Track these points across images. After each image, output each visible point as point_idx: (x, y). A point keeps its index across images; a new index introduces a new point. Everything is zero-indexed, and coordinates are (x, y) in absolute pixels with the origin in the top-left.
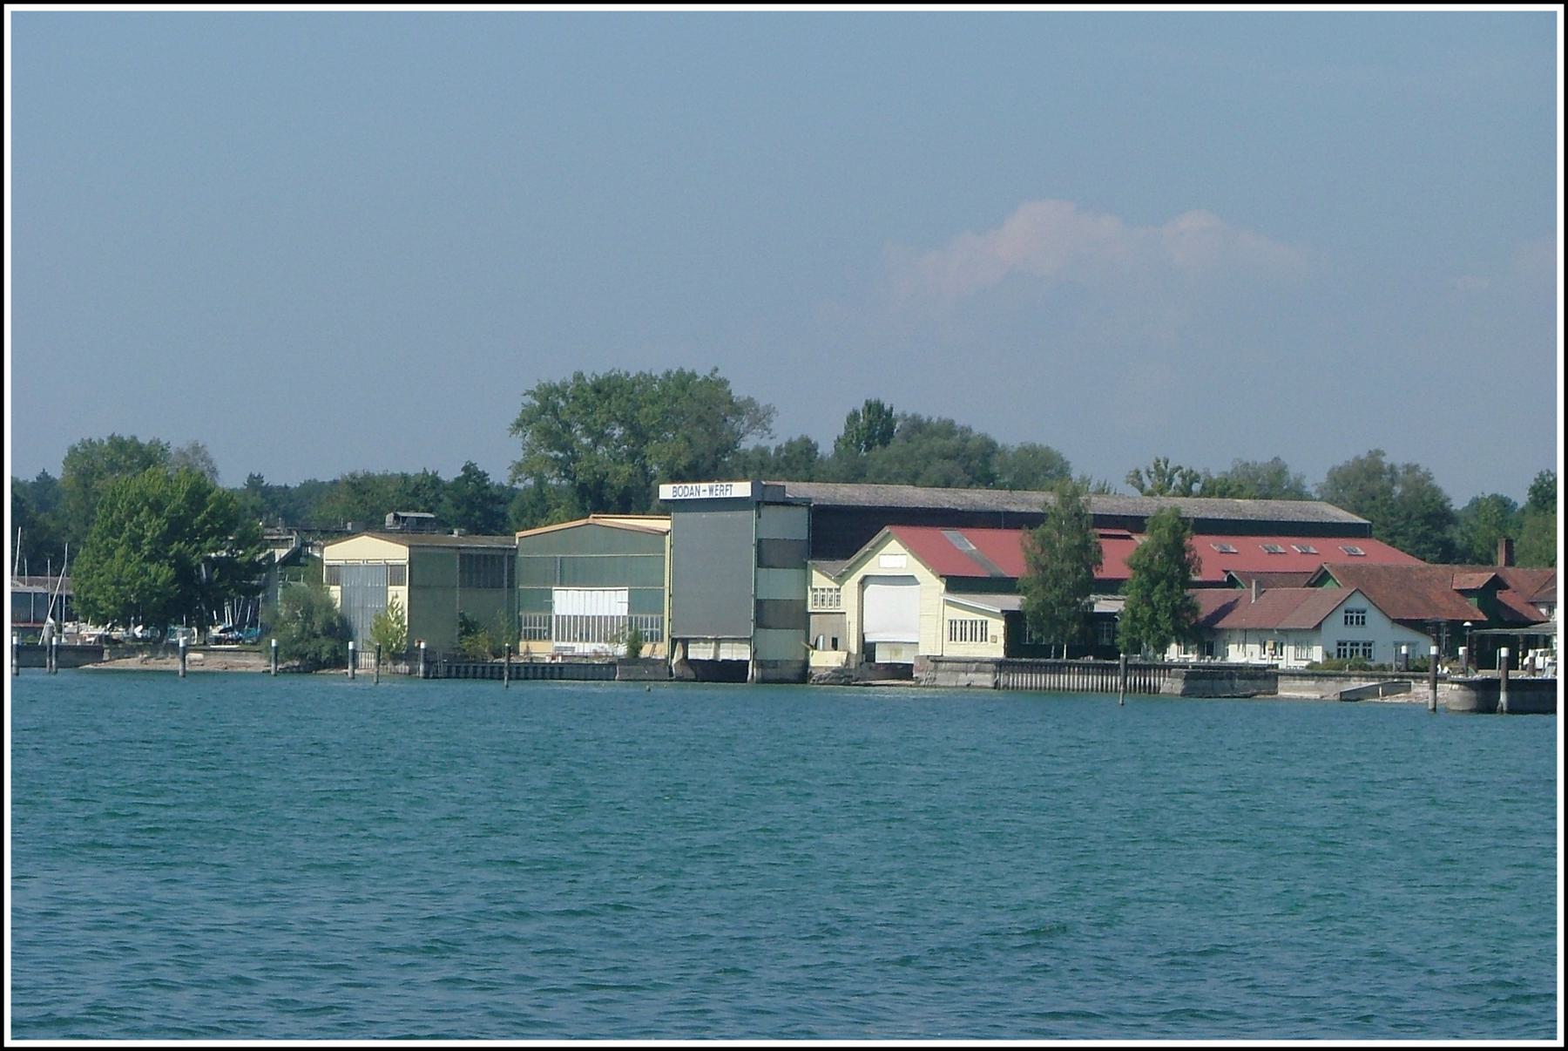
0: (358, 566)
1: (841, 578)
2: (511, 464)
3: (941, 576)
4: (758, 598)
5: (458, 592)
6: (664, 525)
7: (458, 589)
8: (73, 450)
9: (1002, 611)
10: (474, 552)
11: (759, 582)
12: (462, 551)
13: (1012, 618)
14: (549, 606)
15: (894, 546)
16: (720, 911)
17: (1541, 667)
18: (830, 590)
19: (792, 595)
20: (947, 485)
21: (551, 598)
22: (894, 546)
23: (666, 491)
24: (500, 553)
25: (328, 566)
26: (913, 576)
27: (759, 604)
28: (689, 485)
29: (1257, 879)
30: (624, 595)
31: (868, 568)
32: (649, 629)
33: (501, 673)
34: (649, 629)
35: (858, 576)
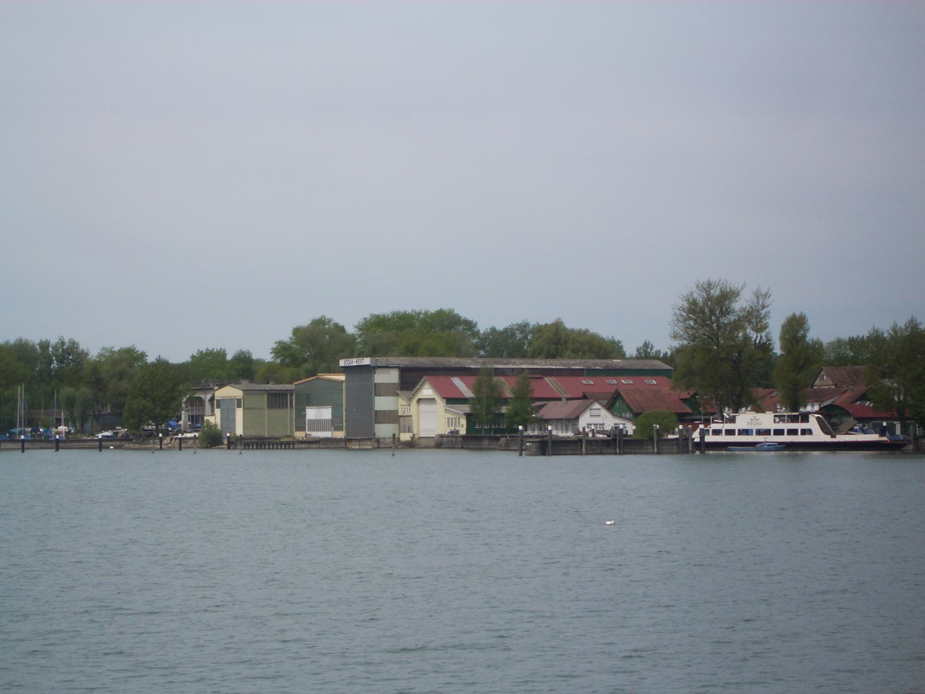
0: (226, 399)
1: (410, 399)
2: (271, 351)
3: (443, 398)
5: (266, 412)
6: (342, 377)
8: (794, 316)
9: (464, 414)
10: (282, 392)
11: (577, 397)
12: (269, 392)
13: (468, 416)
15: (427, 386)
16: (754, 547)
17: (295, 447)
18: (404, 405)
19: (206, 414)
20: (443, 356)
21: (305, 412)
22: (427, 386)
23: (342, 363)
24: (286, 392)
25: (217, 400)
26: (434, 399)
28: (349, 360)
29: (469, 534)
31: (419, 396)
33: (752, 432)
35: (416, 399)
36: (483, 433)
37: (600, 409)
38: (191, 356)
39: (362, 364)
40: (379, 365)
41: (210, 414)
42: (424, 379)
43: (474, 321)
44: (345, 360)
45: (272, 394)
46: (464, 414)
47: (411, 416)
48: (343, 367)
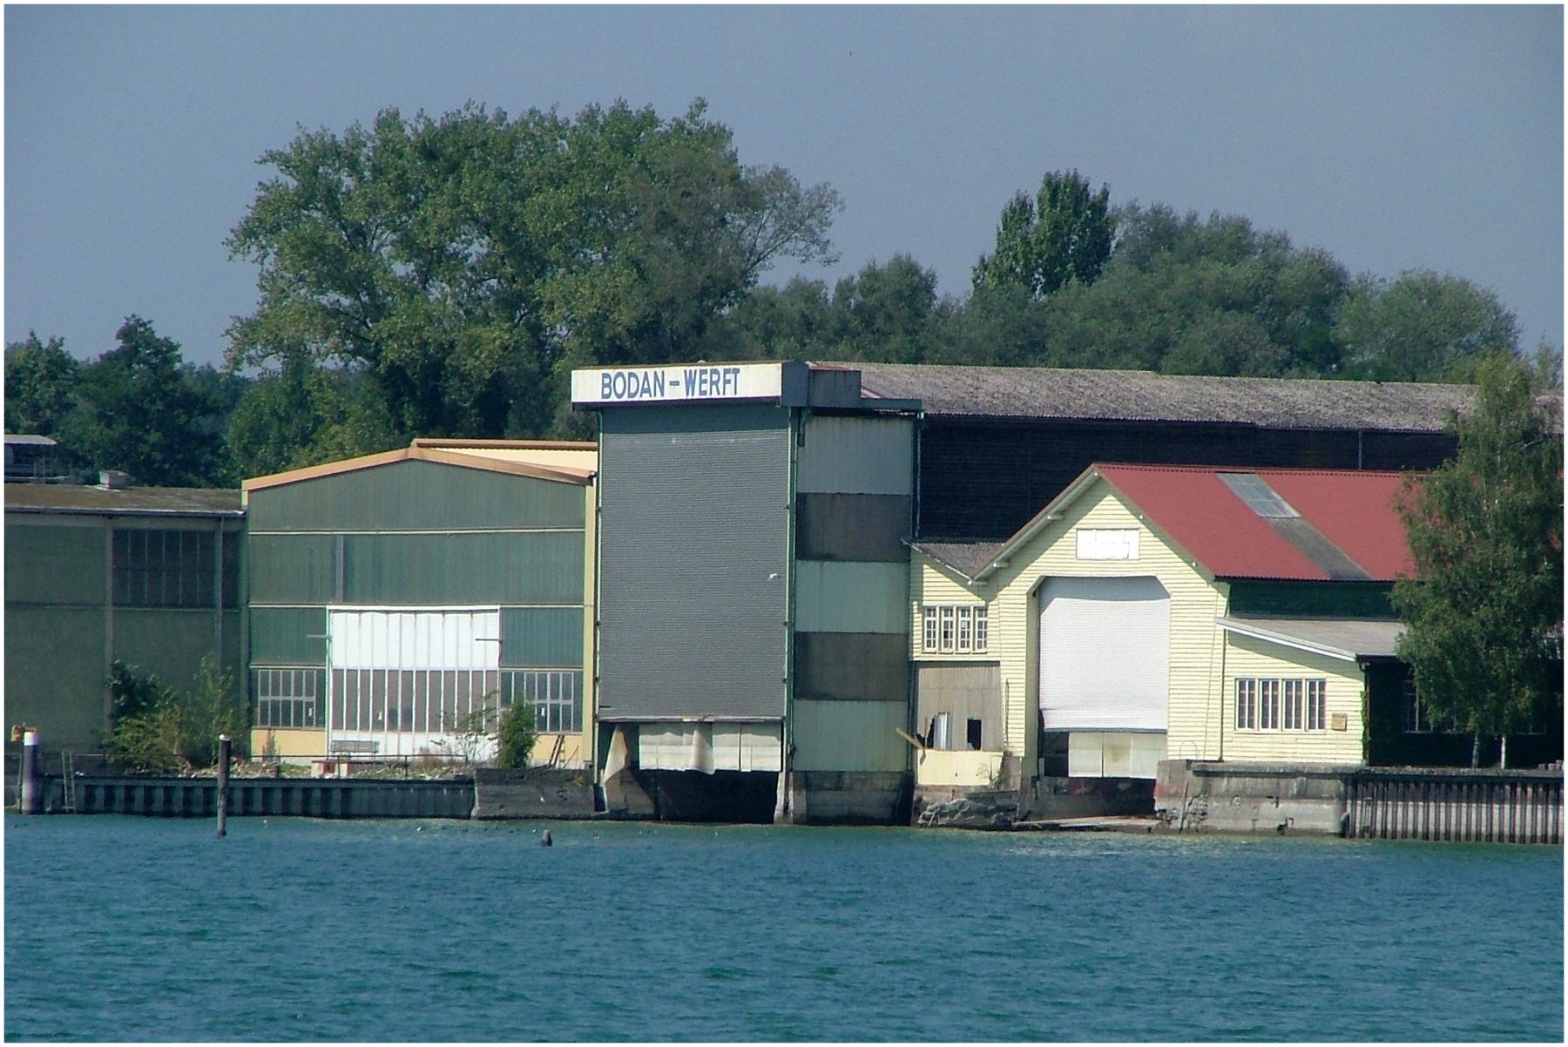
1: (988, 584)
3: (1218, 579)
4: (801, 628)
6: (581, 461)
7: (109, 608)
10: (145, 525)
12: (123, 524)
14: (320, 649)
15: (1110, 509)
22: (1110, 509)
23: (587, 385)
24: (206, 526)
26: (1152, 580)
27: (801, 643)
30: (488, 624)
32: (548, 701)
34: (548, 701)
36: (549, 675)
37: (1146, 587)
38: (782, 167)
39: (729, 394)
40: (820, 401)
41: (300, 812)
42: (1093, 465)
43: (771, 285)
44: (612, 372)
45: (138, 535)
46: (1360, 659)
47: (997, 663)
48: (588, 407)
